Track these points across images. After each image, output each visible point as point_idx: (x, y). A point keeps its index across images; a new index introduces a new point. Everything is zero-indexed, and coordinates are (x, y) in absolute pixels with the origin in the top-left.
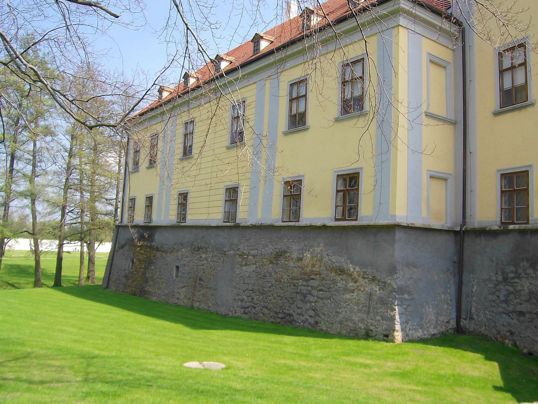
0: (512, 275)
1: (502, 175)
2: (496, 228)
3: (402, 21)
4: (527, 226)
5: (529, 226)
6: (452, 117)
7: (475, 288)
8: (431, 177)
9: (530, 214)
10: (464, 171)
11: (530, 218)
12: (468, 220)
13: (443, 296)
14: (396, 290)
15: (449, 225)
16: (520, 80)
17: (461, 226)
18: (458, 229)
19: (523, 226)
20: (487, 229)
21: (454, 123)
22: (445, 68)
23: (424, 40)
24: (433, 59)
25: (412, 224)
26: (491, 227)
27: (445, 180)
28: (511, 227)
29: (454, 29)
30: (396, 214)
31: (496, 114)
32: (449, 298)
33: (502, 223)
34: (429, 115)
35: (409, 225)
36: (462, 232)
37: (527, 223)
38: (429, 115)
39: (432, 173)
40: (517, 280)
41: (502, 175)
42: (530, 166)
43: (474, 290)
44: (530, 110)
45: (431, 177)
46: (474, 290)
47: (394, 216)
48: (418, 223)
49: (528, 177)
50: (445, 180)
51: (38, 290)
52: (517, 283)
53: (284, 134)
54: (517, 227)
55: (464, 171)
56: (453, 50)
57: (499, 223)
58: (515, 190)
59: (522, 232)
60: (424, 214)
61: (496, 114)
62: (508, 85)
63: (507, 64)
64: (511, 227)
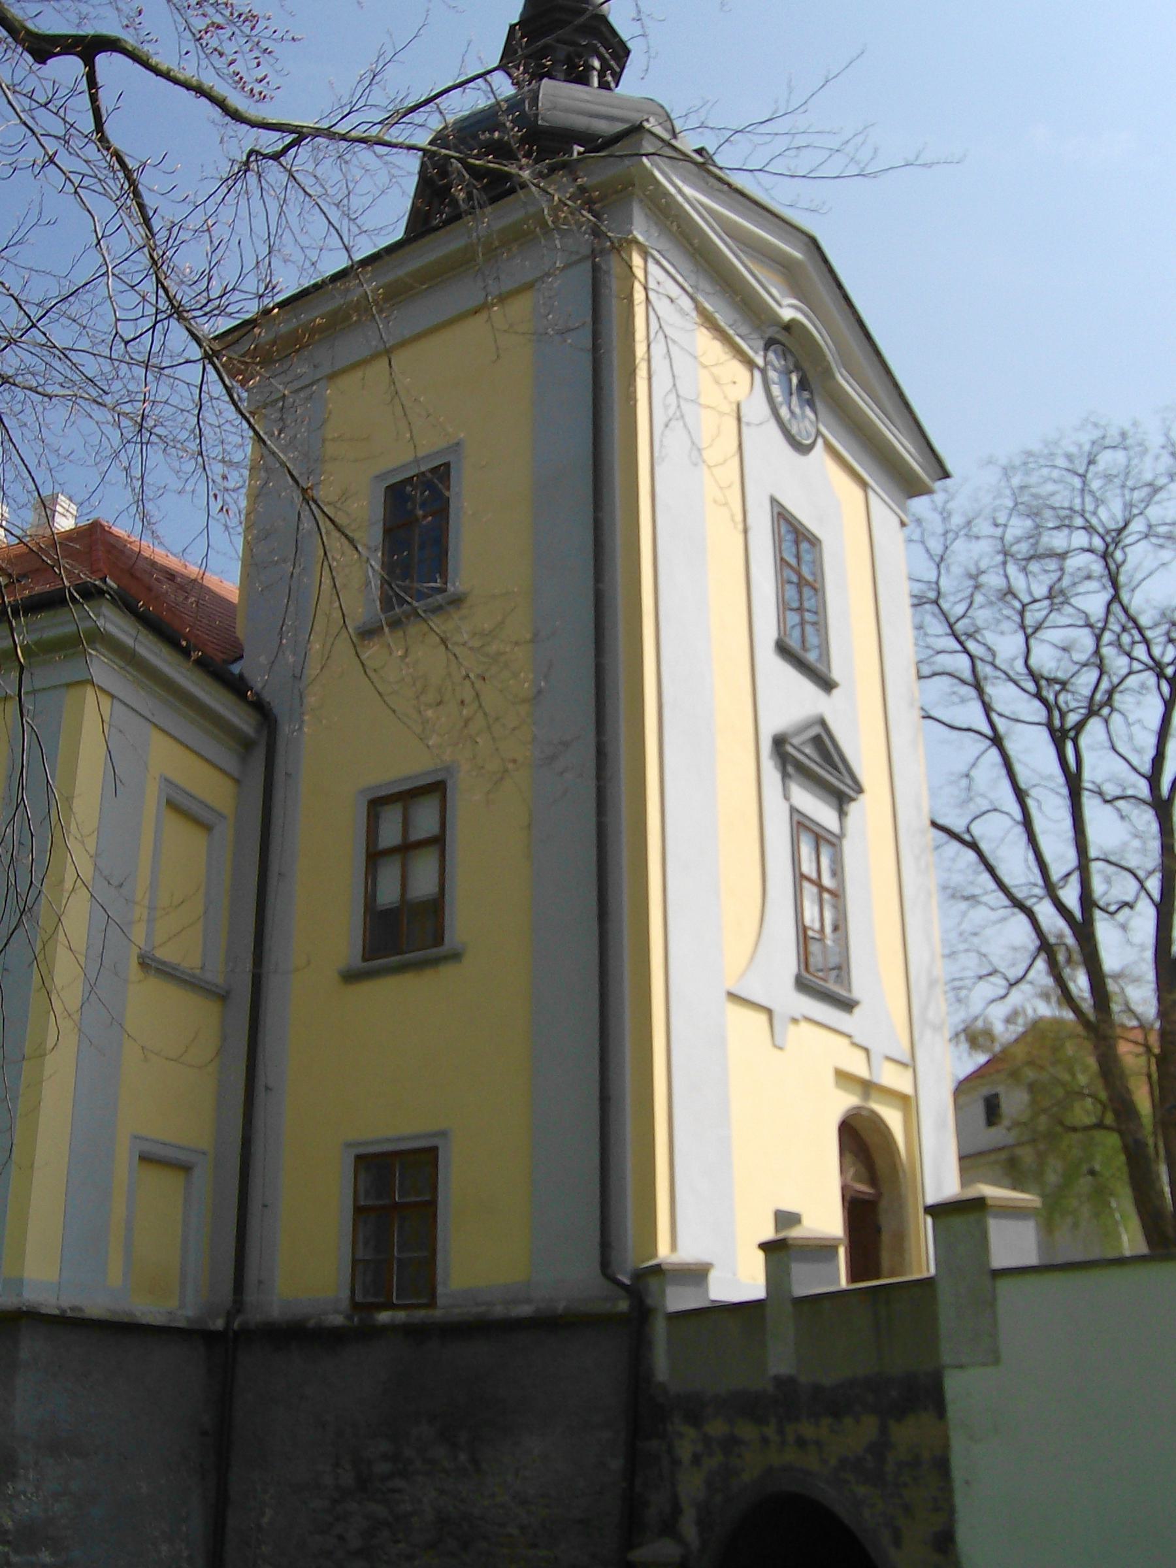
0: (383, 1468)
1: (359, 1158)
2: (338, 1320)
3: (101, 667)
4: (431, 1312)
5: (437, 1314)
6: (216, 976)
7: (269, 1512)
8: (145, 1158)
9: (440, 1278)
10: (247, 1143)
11: (440, 1290)
12: (251, 1296)
13: (164, 1548)
14: (10, 1538)
15: (190, 1312)
16: (424, 883)
17: (230, 1316)
18: (219, 1324)
19: (420, 1315)
20: (311, 1323)
21: (223, 997)
22: (207, 828)
23: (157, 737)
24: (179, 799)
25: (72, 1309)
26: (323, 1317)
27: (186, 1168)
28: (384, 1317)
29: (242, 720)
30: (26, 1275)
31: (351, 977)
32: (185, 1554)
33: (356, 1306)
34: (147, 963)
35: (64, 1311)
36: (231, 1334)
37: (432, 1304)
38: (147, 963)
39: (147, 1147)
40: (399, 1483)
41: (359, 1158)
42: (443, 1134)
43: (265, 1520)
44: (447, 971)
45: (145, 1158)
46: (265, 1520)
47: (18, 1283)
48: (96, 1306)
49: (436, 1166)
50: (186, 1168)
51: (907, 601)
52: (399, 1491)
53: (234, 628)
54: (401, 1316)
55: (247, 1143)
56: (238, 781)
57: (345, 1304)
58: (396, 1206)
59: (415, 1333)
60: (115, 1275)
61: (351, 977)
62: (388, 894)
63: (390, 835)
64: (384, 1317)
